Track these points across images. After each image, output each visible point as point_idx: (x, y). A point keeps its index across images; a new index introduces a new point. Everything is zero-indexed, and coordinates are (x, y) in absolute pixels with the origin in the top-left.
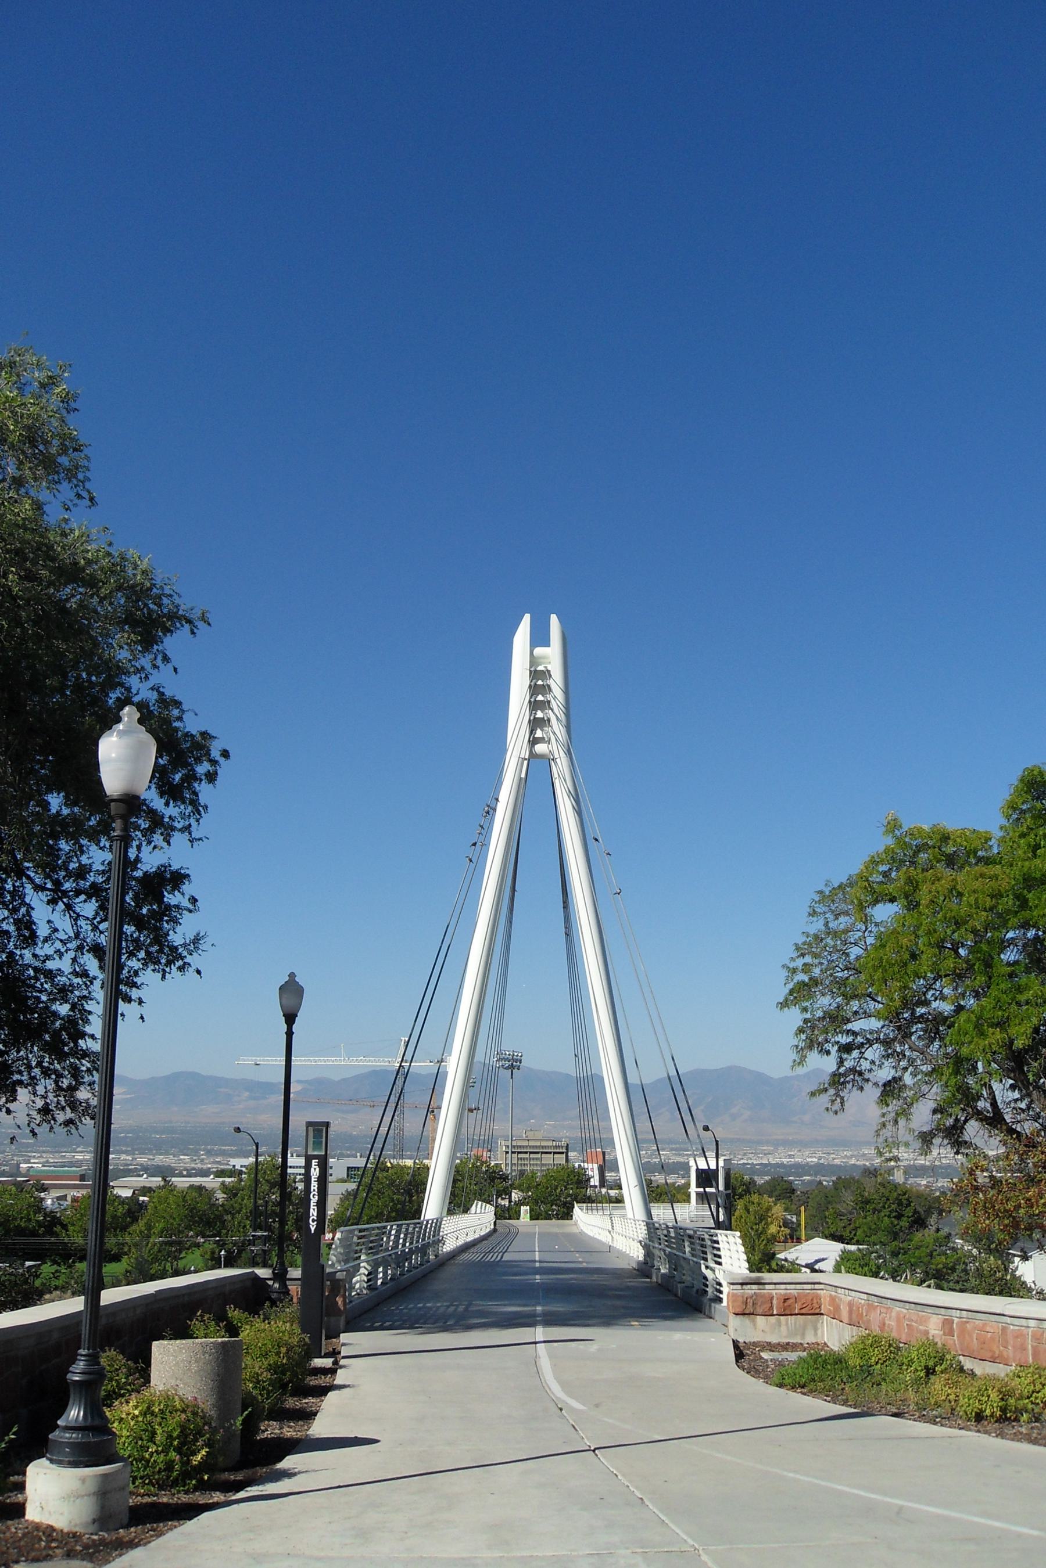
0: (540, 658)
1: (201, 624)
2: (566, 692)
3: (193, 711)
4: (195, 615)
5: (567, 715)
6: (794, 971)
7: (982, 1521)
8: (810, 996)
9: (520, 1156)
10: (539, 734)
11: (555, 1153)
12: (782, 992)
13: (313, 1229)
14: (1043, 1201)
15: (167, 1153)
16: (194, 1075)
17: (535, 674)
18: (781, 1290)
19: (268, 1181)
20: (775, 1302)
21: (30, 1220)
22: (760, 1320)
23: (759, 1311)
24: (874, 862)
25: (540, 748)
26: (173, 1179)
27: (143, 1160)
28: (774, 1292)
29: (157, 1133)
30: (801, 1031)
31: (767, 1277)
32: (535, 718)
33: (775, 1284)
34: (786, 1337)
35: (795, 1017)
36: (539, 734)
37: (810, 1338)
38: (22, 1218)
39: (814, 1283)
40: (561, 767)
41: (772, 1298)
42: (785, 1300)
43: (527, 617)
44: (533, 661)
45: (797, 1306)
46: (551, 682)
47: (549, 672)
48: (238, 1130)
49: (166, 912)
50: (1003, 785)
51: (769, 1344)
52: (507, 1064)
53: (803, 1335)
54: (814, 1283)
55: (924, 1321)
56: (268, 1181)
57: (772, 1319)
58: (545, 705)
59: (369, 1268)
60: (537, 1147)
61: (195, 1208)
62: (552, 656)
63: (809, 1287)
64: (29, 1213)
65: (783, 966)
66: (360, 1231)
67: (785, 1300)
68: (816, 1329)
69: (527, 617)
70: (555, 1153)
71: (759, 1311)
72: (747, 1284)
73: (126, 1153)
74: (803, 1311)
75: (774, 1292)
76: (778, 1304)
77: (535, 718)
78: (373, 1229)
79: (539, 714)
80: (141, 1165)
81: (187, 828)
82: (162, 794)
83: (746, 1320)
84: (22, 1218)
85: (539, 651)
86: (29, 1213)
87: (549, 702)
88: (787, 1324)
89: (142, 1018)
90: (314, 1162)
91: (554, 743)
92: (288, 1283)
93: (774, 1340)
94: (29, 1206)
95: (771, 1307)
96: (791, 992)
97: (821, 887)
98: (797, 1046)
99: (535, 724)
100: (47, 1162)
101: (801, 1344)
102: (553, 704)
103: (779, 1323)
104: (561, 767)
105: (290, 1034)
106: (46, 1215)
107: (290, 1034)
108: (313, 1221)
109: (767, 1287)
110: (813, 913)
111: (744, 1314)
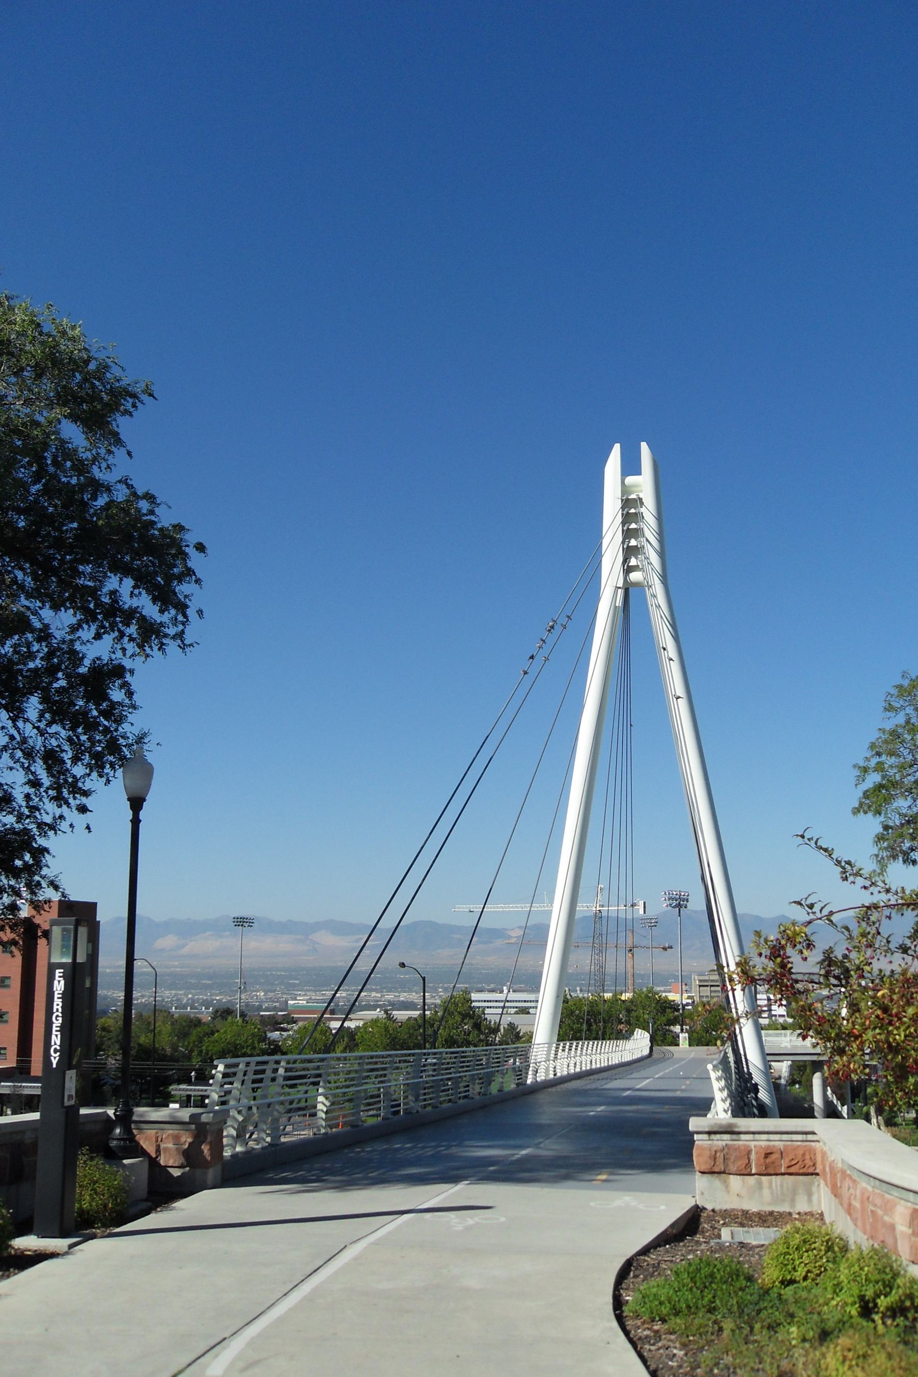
1: (145, 397)
2: (659, 518)
3: (167, 505)
4: (138, 389)
5: (661, 541)
6: (865, 770)
8: (888, 800)
9: (713, 989)
10: (633, 562)
11: (711, 986)
12: (855, 796)
14: (911, 1011)
15: (410, 991)
16: (431, 924)
17: (627, 503)
18: (762, 1142)
19: (459, 1013)
20: (753, 1157)
21: (254, 1048)
22: (735, 1181)
23: (733, 1169)
25: (635, 576)
26: (394, 1012)
28: (752, 1144)
30: (880, 838)
31: (744, 1123)
32: (628, 546)
33: (754, 1133)
34: (769, 1204)
35: (872, 824)
36: (633, 562)
37: (802, 1206)
38: (247, 1046)
39: (806, 1133)
41: (749, 1152)
42: (767, 1155)
43: (617, 447)
44: (625, 490)
45: (784, 1163)
46: (643, 510)
47: (641, 499)
48: (403, 965)
49: (113, 713)
51: (745, 1213)
52: (675, 903)
53: (793, 1201)
54: (806, 1133)
55: (889, 1208)
56: (459, 1013)
57: (751, 1180)
58: (636, 534)
59: (328, 1104)
60: (706, 981)
61: (396, 1038)
62: (643, 484)
63: (800, 1137)
64: (253, 1042)
65: (855, 766)
66: (258, 1063)
67: (767, 1155)
68: (810, 1195)
69: (617, 447)
70: (711, 986)
71: (733, 1169)
72: (715, 1133)
73: (376, 991)
74: (792, 1170)
75: (752, 1144)
76: (758, 1159)
77: (628, 546)
78: (397, 1056)
79: (633, 542)
80: (389, 1001)
81: (180, 635)
82: (154, 600)
83: (716, 1181)
84: (247, 1046)
85: (630, 480)
86: (253, 1042)
88: (770, 1187)
89: (88, 828)
90: (58, 973)
91: (649, 571)
92: (133, 1126)
93: (754, 1207)
94: (253, 1035)
95: (749, 1164)
96: (866, 794)
97: (900, 681)
98: (877, 856)
99: (629, 552)
100: (310, 999)
101: (790, 1214)
103: (760, 1185)
105: (136, 822)
106: (270, 1044)
107: (136, 822)
108: (56, 1051)
109: (743, 1137)
110: (890, 708)
111: (714, 1173)
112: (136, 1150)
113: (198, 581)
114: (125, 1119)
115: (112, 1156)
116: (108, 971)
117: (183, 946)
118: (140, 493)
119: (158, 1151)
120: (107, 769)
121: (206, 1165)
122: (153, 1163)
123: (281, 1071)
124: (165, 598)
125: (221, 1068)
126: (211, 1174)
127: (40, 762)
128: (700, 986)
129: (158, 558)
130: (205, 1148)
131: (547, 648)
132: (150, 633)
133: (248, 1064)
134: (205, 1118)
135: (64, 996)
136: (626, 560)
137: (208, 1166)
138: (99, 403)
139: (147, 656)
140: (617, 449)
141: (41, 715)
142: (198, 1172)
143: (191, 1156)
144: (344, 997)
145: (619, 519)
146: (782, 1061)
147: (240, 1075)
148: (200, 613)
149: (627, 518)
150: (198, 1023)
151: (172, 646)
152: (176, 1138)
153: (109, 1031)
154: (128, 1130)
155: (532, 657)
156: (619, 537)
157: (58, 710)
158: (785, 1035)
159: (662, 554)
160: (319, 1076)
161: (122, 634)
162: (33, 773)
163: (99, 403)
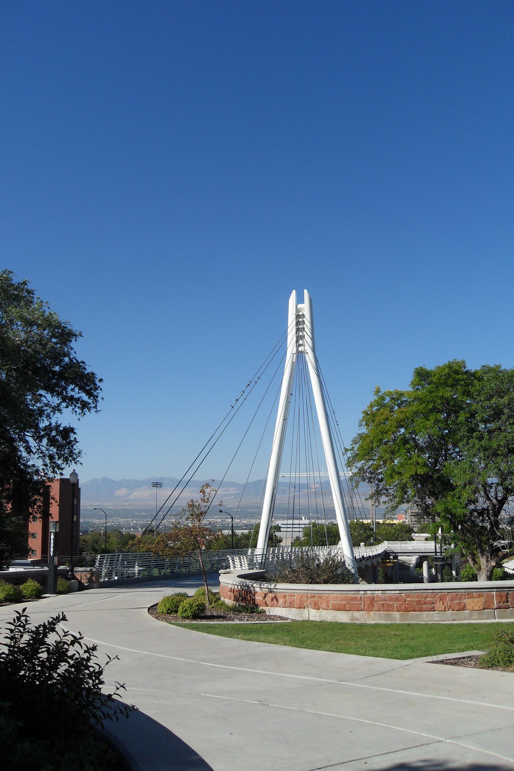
0: (301, 309)
2: (312, 323)
7: (136, 651)
10: (301, 342)
13: (52, 555)
17: (298, 316)
24: (372, 406)
26: (237, 531)
27: (245, 521)
29: (252, 509)
36: (301, 342)
40: (310, 358)
43: (294, 291)
44: (297, 310)
46: (305, 319)
47: (303, 315)
50: (410, 376)
62: (305, 308)
69: (294, 291)
79: (301, 334)
80: (244, 524)
81: (95, 407)
85: (300, 306)
87: (304, 328)
90: (52, 534)
102: (306, 329)
104: (310, 358)
112: (75, 578)
113: (101, 389)
114: (72, 570)
115: (68, 579)
116: (89, 508)
117: (130, 494)
118: (80, 361)
119: (81, 579)
120: (69, 462)
121: (94, 582)
122: (80, 582)
123: (120, 558)
124: (89, 393)
125: (99, 557)
126: (95, 585)
127: (47, 458)
128: (411, 516)
129: (87, 382)
130: (94, 578)
131: (245, 395)
132: (85, 405)
133: (108, 556)
134: (94, 570)
135: (54, 539)
136: (297, 341)
137: (95, 582)
138: (66, 336)
139: (85, 414)
140: (294, 292)
141: (47, 445)
142: (92, 584)
143: (90, 580)
144: (219, 522)
145: (294, 323)
146: (412, 556)
147: (106, 559)
148: (102, 398)
149: (298, 323)
150: (133, 537)
151: (93, 411)
152: (86, 575)
153: (87, 542)
154: (72, 573)
155: (237, 400)
156: (294, 330)
157: (52, 442)
158: (398, 543)
159: (313, 339)
160: (136, 559)
161: (75, 406)
162: (46, 462)
163: (66, 336)
